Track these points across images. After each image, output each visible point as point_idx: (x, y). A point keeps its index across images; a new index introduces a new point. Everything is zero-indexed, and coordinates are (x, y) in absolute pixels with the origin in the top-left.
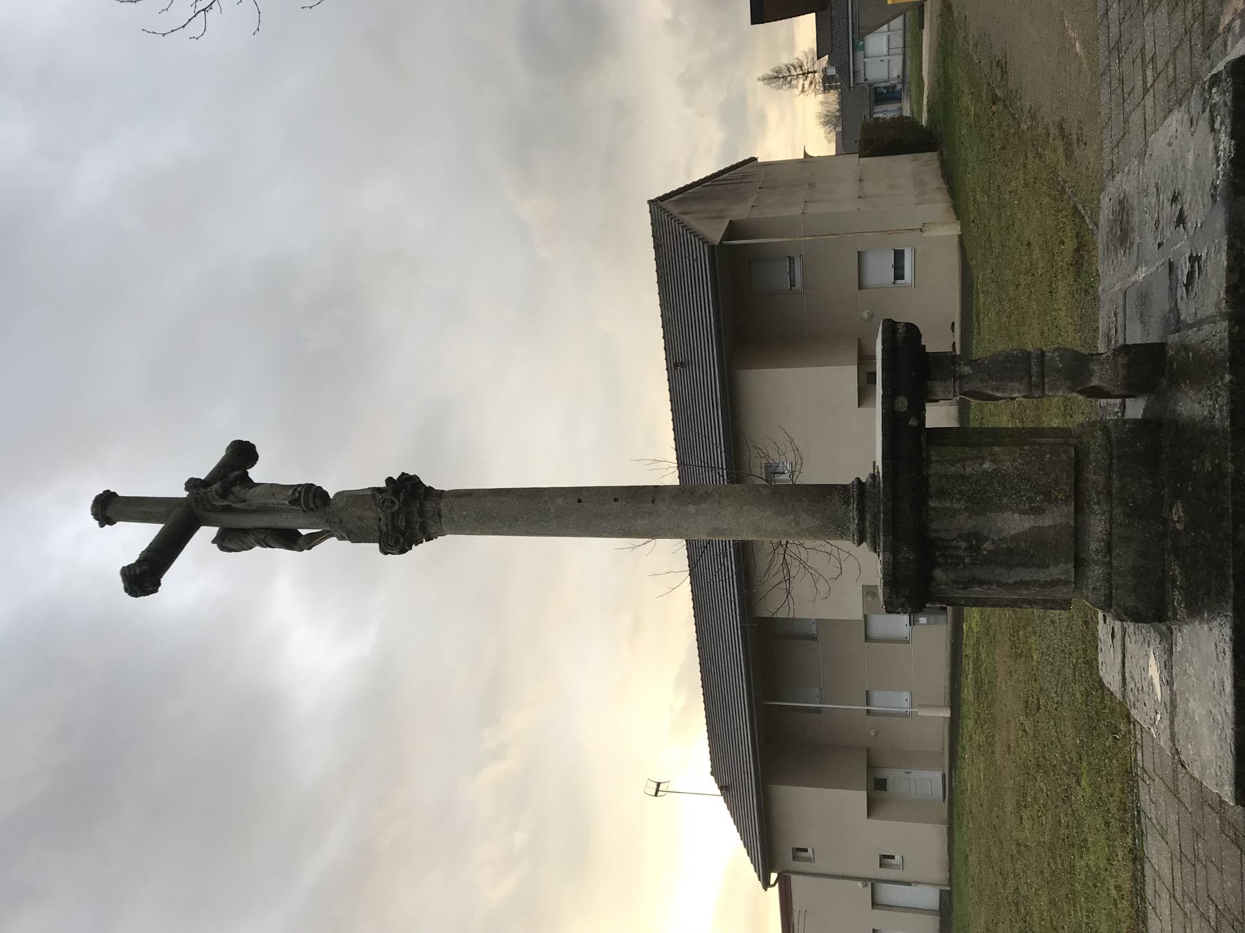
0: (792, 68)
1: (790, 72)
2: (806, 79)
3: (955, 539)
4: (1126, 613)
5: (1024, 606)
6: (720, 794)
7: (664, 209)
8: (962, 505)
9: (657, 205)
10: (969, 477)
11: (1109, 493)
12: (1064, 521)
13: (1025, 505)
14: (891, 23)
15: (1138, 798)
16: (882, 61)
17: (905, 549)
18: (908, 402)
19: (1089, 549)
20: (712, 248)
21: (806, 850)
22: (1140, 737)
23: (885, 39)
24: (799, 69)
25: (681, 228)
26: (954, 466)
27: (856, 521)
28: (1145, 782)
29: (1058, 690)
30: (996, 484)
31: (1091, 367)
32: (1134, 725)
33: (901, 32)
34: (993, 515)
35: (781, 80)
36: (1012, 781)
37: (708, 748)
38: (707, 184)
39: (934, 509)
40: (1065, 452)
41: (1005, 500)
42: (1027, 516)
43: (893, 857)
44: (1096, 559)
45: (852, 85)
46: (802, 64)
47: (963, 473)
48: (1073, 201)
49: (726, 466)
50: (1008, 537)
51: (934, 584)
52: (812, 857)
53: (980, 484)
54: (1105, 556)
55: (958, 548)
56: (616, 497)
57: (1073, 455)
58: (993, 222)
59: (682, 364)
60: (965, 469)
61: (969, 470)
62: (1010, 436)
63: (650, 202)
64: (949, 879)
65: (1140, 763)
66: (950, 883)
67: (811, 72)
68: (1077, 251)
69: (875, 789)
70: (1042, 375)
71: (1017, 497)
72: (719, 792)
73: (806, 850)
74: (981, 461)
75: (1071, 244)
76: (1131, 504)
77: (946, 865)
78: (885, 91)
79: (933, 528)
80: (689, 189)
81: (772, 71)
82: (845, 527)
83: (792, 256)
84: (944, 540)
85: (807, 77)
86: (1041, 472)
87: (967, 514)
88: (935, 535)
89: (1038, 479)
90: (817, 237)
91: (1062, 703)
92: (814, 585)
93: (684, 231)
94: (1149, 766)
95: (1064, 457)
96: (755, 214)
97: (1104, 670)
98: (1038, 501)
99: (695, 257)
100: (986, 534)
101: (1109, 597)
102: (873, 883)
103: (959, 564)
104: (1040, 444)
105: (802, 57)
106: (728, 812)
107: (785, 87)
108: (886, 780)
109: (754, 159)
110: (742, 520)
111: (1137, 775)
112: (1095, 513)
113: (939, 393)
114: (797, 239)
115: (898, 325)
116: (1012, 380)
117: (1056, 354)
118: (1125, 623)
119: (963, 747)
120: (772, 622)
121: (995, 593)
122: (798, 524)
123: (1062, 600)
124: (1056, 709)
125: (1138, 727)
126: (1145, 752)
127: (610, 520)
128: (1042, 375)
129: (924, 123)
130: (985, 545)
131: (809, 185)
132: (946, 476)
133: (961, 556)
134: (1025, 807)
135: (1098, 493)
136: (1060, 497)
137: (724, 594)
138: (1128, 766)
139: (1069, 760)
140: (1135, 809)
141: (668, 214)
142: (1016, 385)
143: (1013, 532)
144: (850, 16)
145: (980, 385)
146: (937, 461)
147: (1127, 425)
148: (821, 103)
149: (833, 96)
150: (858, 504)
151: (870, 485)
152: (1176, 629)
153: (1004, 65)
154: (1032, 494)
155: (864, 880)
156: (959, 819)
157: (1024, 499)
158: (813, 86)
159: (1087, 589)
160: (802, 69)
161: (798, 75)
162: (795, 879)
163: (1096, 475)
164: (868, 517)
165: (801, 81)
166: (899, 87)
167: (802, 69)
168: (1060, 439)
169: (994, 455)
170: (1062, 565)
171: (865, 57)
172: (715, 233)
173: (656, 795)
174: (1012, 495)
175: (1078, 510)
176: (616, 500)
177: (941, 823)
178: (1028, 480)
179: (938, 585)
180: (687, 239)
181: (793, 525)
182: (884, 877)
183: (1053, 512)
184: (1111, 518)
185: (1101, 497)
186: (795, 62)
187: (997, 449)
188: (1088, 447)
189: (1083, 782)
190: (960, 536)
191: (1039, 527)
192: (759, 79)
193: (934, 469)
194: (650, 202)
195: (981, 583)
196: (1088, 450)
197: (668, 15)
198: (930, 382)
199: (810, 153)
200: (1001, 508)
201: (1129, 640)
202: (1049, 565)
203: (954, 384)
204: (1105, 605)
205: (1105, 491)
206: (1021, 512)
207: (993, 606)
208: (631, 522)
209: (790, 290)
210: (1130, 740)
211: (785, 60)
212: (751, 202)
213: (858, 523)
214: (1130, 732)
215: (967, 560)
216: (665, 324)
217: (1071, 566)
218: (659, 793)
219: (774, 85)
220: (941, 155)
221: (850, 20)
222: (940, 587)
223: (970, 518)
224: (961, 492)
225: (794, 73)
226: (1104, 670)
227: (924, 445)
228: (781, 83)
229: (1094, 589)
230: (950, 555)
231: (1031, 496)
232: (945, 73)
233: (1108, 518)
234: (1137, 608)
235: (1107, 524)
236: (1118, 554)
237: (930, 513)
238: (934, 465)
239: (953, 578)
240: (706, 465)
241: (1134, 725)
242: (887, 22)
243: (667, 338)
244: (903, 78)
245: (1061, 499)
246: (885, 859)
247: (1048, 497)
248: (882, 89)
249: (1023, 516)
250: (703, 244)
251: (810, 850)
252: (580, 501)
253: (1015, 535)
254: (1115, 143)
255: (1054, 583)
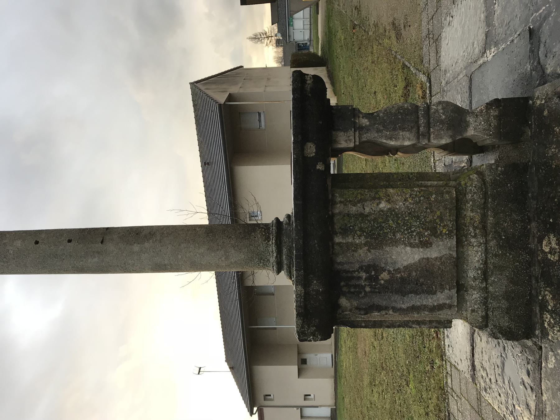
0: (262, 34)
1: (261, 36)
2: (268, 40)
3: (357, 271)
4: (501, 332)
5: (413, 326)
6: (230, 371)
7: (197, 87)
8: (363, 240)
9: (194, 85)
10: (367, 216)
11: (484, 228)
12: (448, 253)
13: (415, 240)
14: (304, 10)
15: (448, 404)
16: (301, 32)
17: (315, 282)
18: (316, 148)
19: (467, 276)
20: (220, 105)
21: (270, 395)
22: (450, 370)
23: (302, 22)
24: (265, 35)
25: (205, 96)
26: (354, 206)
27: (275, 255)
28: (454, 398)
29: (395, 331)
30: (391, 222)
31: (468, 119)
32: (446, 362)
33: (309, 20)
34: (388, 249)
35: (257, 39)
36: (367, 370)
37: (224, 349)
38: (219, 76)
39: (339, 244)
40: (448, 192)
41: (398, 236)
42: (417, 249)
43: (310, 395)
44: (474, 284)
45: (288, 42)
46: (266, 33)
47: (363, 212)
48: (402, 61)
49: (230, 215)
50: (402, 268)
51: (340, 311)
52: (273, 398)
53: (378, 222)
54: (482, 283)
55: (360, 278)
56: (38, 240)
57: (455, 195)
58: (354, 89)
59: (208, 163)
60: (364, 209)
61: (367, 210)
62: (400, 180)
63: (191, 84)
64: (335, 403)
65: (450, 385)
66: (336, 405)
67: (270, 37)
68: (406, 87)
69: (301, 364)
70: (428, 126)
71: (409, 233)
72: (229, 370)
73: (270, 395)
74: (378, 202)
75: (401, 85)
76: (504, 237)
77: (334, 397)
78: (302, 46)
79: (339, 261)
80: (210, 79)
81: (253, 35)
82: (266, 260)
83: (259, 112)
84: (349, 272)
85: (268, 39)
86: (428, 211)
87: (367, 248)
88: (340, 267)
89: (426, 217)
90: (270, 102)
91: (397, 339)
92: (267, 276)
93: (207, 97)
94: (456, 388)
95: (447, 196)
96: (242, 91)
97: (451, 352)
98: (426, 236)
99: (212, 110)
100: (383, 265)
101: (486, 318)
102: (301, 408)
103: (361, 293)
104: (426, 186)
105: (267, 30)
106: (234, 379)
107: (259, 43)
108: (306, 359)
109: (242, 67)
110: (180, 257)
111: (447, 391)
112: (473, 245)
113: (342, 142)
114: (261, 103)
115: (306, 76)
116: (403, 129)
117: (440, 107)
118: (499, 340)
119: (341, 345)
120: (252, 288)
121: (392, 316)
122: (227, 258)
123: (444, 321)
124: (393, 341)
125: (448, 364)
126: (453, 379)
127: (64, 259)
128: (428, 126)
129: (319, 55)
130: (382, 275)
131: (267, 79)
132: (348, 215)
133: (362, 285)
134: (375, 385)
135: (475, 228)
136: (444, 232)
137: (230, 276)
138: (442, 385)
139: (401, 370)
140: (447, 412)
141: (199, 89)
142: (407, 134)
143: (405, 264)
144: (287, 6)
145: (376, 135)
146: (341, 202)
147: (500, 169)
148: (275, 52)
149: (281, 49)
150: (276, 241)
151: (286, 224)
152: (546, 348)
153: (359, 8)
154: (421, 230)
155: (297, 407)
156: (340, 379)
157: (415, 234)
158: (271, 43)
159: (466, 311)
160: (266, 35)
161: (264, 37)
162: (265, 410)
163: (473, 212)
164: (285, 251)
165: (266, 40)
166: (308, 44)
167: (266, 35)
168: (442, 182)
169: (389, 196)
170: (447, 291)
171: (293, 30)
172: (222, 99)
173: (199, 374)
174: (404, 230)
175: (459, 243)
176: (70, 241)
177: (331, 378)
178: (418, 217)
179: (343, 312)
180: (208, 101)
181: (223, 259)
182: (307, 405)
183: (439, 245)
184: (486, 249)
185: (478, 231)
186: (263, 32)
187: (391, 190)
188: (466, 188)
189: (410, 385)
190: (361, 268)
191: (428, 259)
192: (247, 38)
193: (339, 208)
194: (191, 84)
195: (379, 308)
196: (466, 191)
197: (207, 11)
198: (334, 133)
199: (267, 67)
200: (395, 243)
201: (479, 338)
202: (436, 291)
203: (355, 134)
204: (483, 325)
205: (480, 226)
206: (412, 246)
207: (388, 327)
208: (82, 261)
209: (259, 128)
210: (443, 370)
211: (259, 30)
212: (240, 85)
213: (276, 257)
214: (443, 366)
215: (368, 289)
216: (200, 144)
217: (454, 291)
218: (200, 373)
219: (254, 41)
220: (328, 68)
221: (287, 8)
222: (345, 313)
223: (370, 252)
224: (361, 229)
225: (263, 36)
226: (451, 352)
227: (330, 188)
228: (257, 41)
229: (473, 311)
230: (353, 285)
231: (421, 232)
232: (329, 28)
233: (484, 250)
234: (510, 328)
235: (483, 255)
236: (494, 281)
237: (336, 247)
238: (338, 206)
239: (356, 305)
240: (221, 216)
241: (446, 362)
242: (303, 9)
243: (201, 151)
244: (310, 40)
245: (445, 234)
246: (306, 397)
247: (434, 233)
248: (301, 45)
249: (414, 249)
250: (216, 103)
251: (272, 395)
252: (37, 243)
253: (407, 265)
254: (430, 18)
255: (441, 307)
